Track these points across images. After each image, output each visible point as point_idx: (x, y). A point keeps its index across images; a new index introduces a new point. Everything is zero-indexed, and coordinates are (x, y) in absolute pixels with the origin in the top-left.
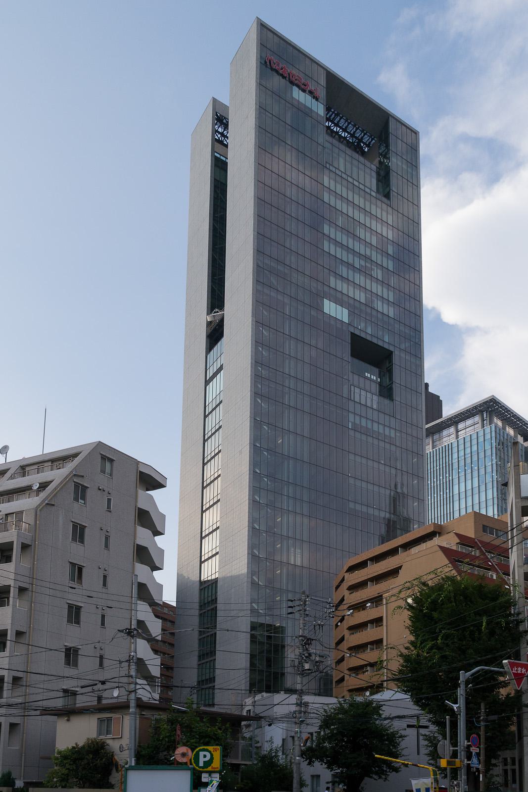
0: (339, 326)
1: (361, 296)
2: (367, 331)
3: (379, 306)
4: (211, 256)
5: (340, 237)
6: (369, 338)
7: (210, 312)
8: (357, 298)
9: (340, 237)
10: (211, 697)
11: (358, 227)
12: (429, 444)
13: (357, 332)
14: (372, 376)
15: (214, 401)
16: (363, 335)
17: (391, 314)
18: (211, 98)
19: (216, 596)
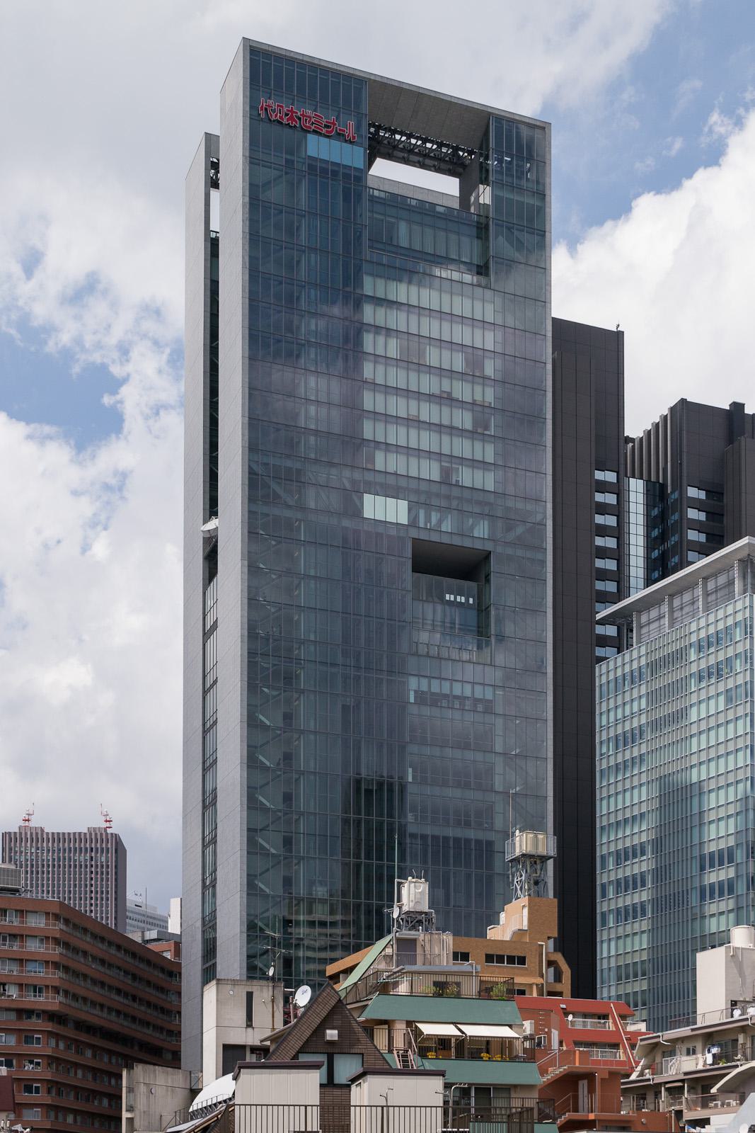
0: (393, 532)
1: (431, 471)
2: (444, 528)
3: (466, 477)
4: (208, 362)
5: (397, 377)
6: (446, 540)
7: (208, 516)
8: (424, 475)
9: (397, 377)
10: (697, 792)
11: (428, 347)
12: (664, 616)
13: (423, 536)
14: (458, 598)
15: (211, 719)
16: (435, 537)
17: (490, 486)
18: (203, 133)
19: (410, 150)
